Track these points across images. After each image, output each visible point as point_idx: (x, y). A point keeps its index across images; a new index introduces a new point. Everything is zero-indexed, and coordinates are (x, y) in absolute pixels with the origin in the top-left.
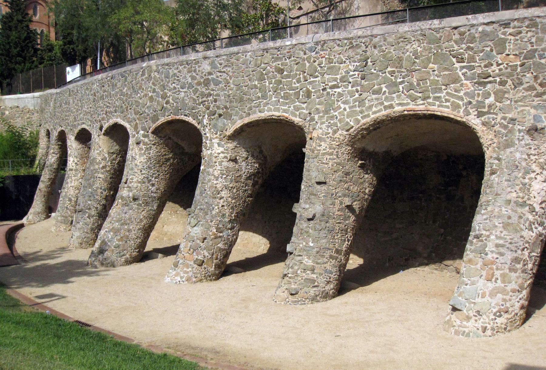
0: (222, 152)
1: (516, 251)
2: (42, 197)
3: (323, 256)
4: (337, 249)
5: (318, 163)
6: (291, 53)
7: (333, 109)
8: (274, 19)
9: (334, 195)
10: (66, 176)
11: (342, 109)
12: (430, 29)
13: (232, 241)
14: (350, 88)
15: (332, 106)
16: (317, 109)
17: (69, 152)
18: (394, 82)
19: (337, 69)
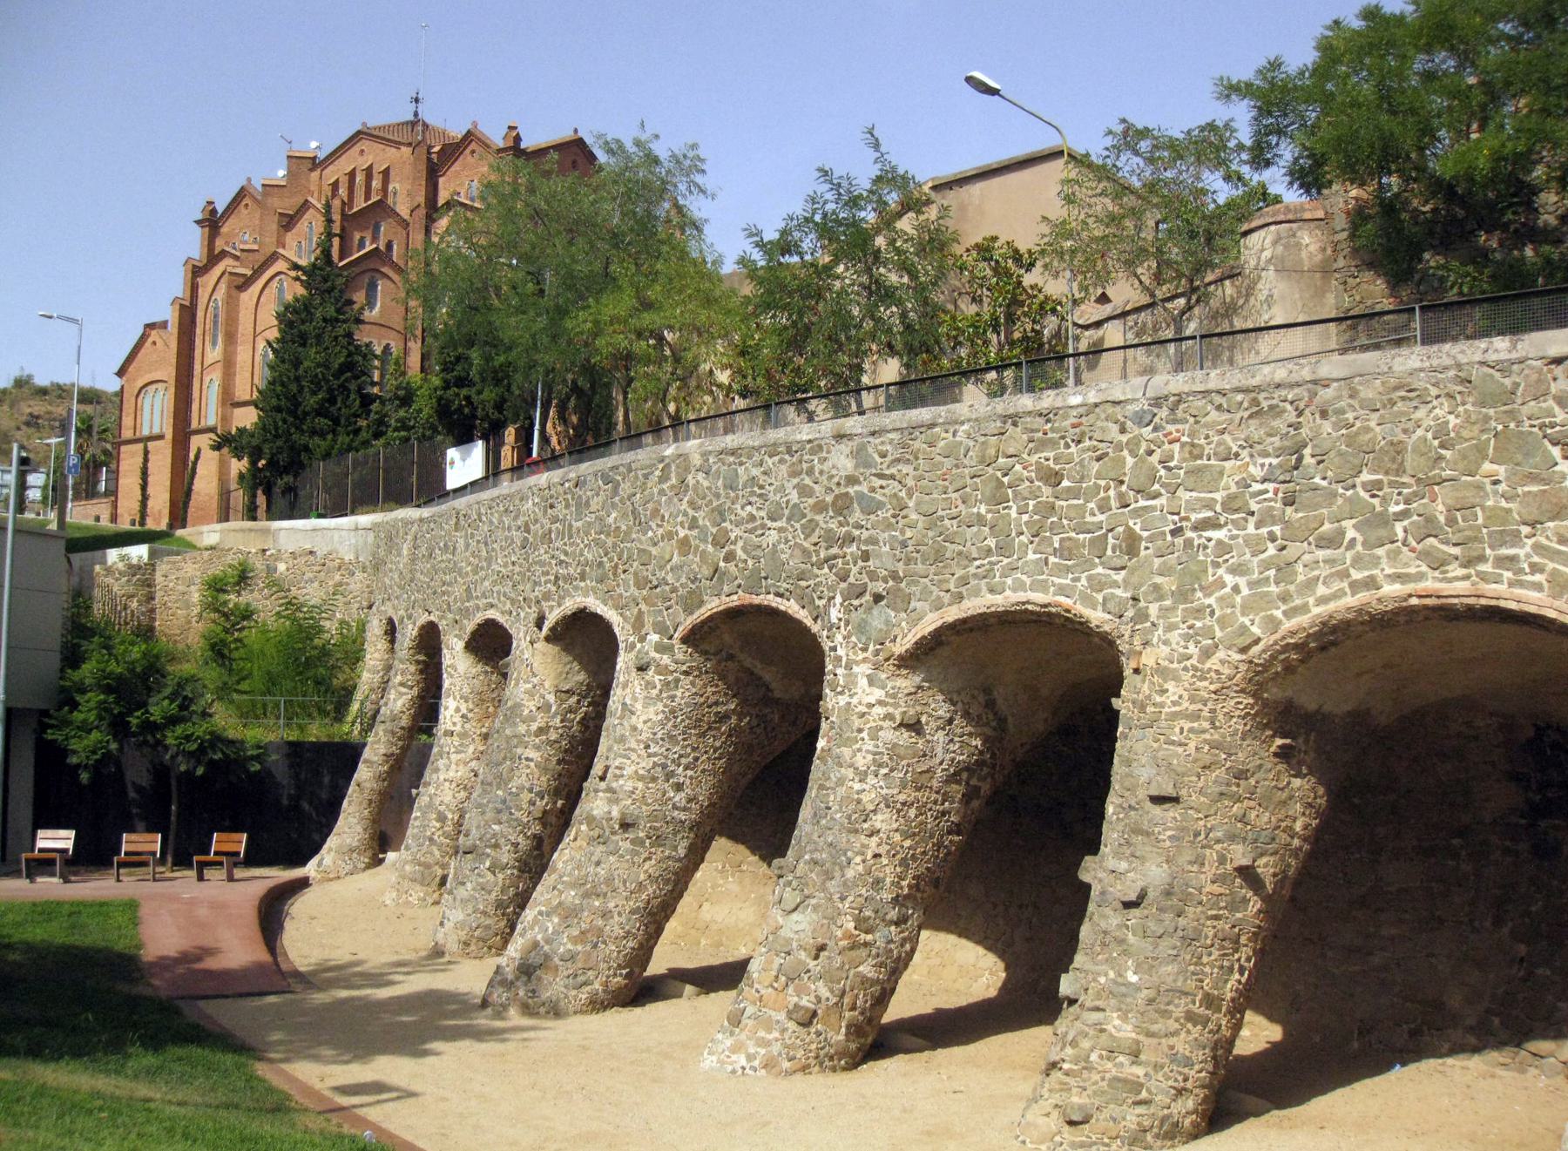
0: (880, 703)
2: (365, 804)
3: (1165, 1014)
4: (1208, 994)
5: (1157, 741)
6: (1083, 428)
7: (1202, 588)
8: (1029, 327)
9: (1203, 836)
10: (435, 750)
11: (1228, 590)
12: (1482, 363)
13: (899, 957)
14: (1251, 529)
15: (1198, 579)
16: (1156, 587)
17: (446, 684)
18: (1381, 514)
19: (1216, 476)
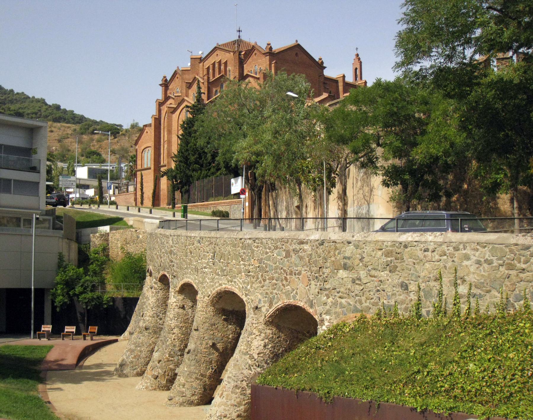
0: (175, 302)
1: (237, 382)
3: (191, 377)
